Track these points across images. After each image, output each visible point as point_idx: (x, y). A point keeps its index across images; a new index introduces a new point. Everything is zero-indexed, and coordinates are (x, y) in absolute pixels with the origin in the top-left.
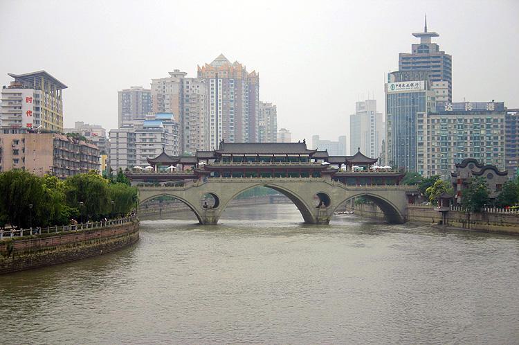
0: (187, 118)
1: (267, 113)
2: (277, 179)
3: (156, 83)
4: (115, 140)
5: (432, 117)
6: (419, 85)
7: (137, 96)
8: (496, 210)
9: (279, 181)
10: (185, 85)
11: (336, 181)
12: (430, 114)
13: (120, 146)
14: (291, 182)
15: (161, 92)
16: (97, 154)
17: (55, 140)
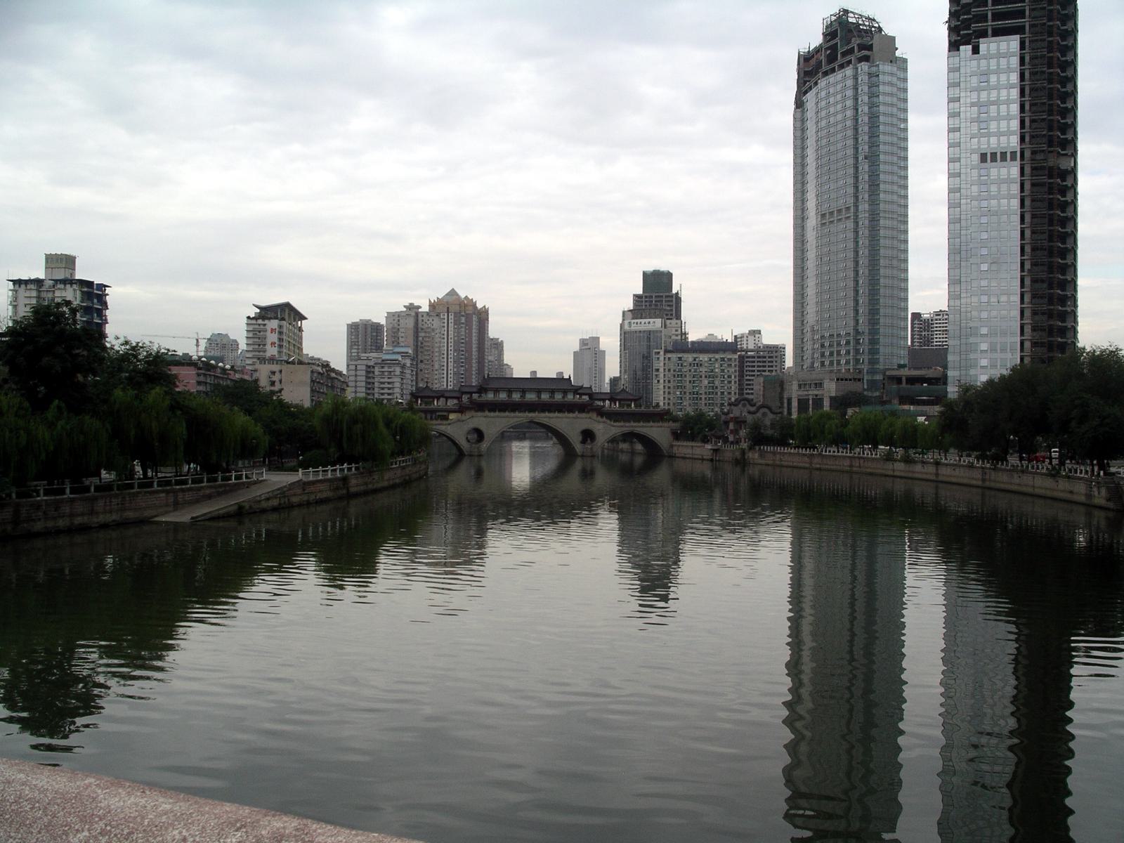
0: (421, 352)
1: (495, 348)
2: (543, 415)
3: (391, 316)
4: (353, 373)
5: (669, 355)
6: (656, 323)
7: (366, 329)
8: (774, 449)
9: (544, 417)
10: (420, 318)
11: (602, 417)
12: (666, 351)
13: (359, 378)
14: (498, 417)
15: (396, 325)
16: (344, 386)
17: (312, 372)
